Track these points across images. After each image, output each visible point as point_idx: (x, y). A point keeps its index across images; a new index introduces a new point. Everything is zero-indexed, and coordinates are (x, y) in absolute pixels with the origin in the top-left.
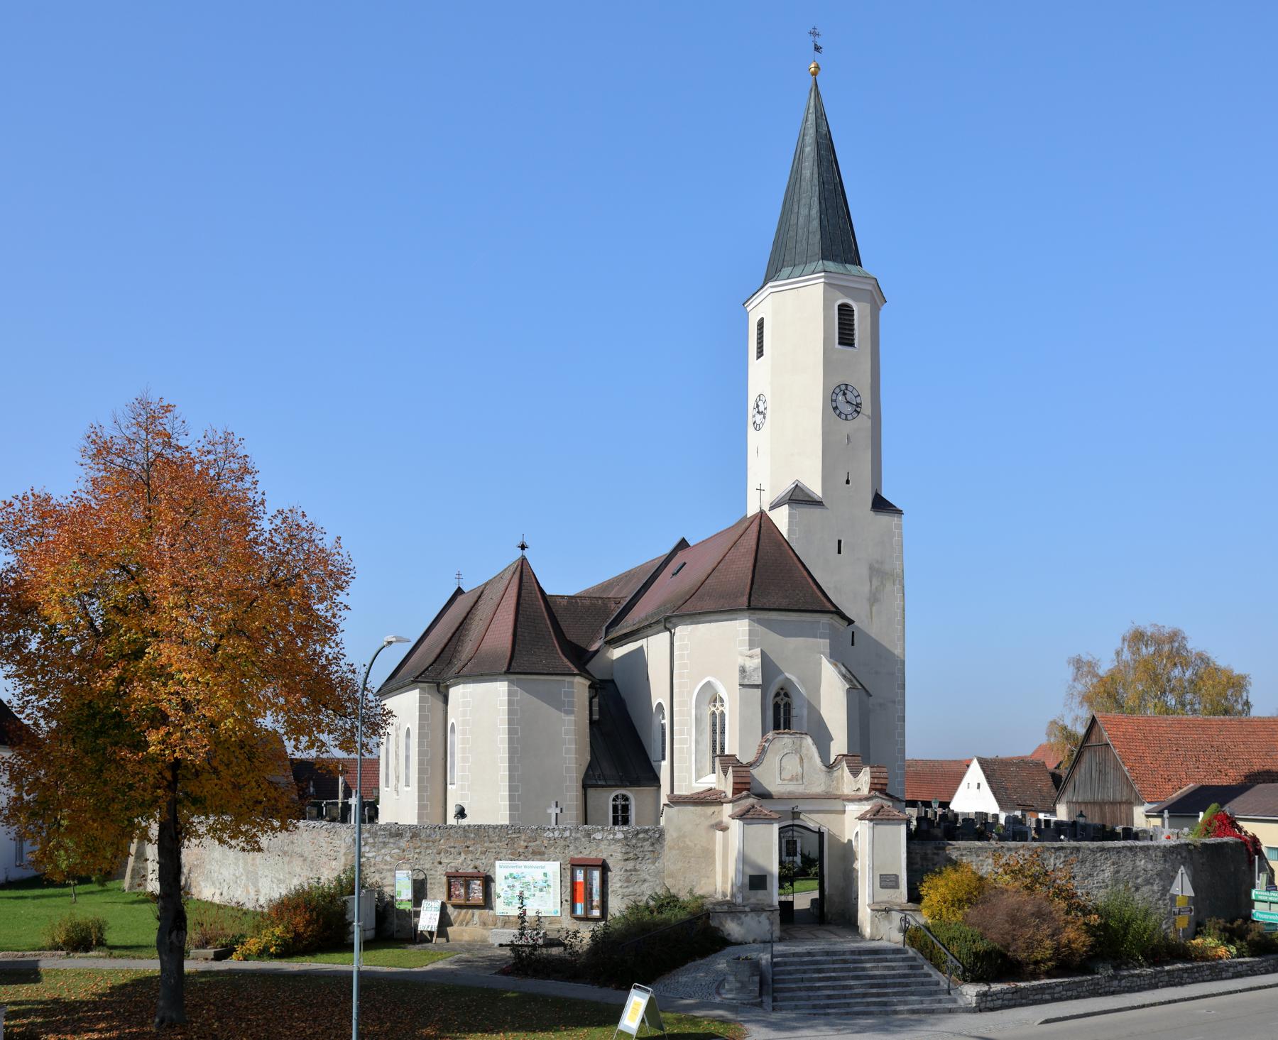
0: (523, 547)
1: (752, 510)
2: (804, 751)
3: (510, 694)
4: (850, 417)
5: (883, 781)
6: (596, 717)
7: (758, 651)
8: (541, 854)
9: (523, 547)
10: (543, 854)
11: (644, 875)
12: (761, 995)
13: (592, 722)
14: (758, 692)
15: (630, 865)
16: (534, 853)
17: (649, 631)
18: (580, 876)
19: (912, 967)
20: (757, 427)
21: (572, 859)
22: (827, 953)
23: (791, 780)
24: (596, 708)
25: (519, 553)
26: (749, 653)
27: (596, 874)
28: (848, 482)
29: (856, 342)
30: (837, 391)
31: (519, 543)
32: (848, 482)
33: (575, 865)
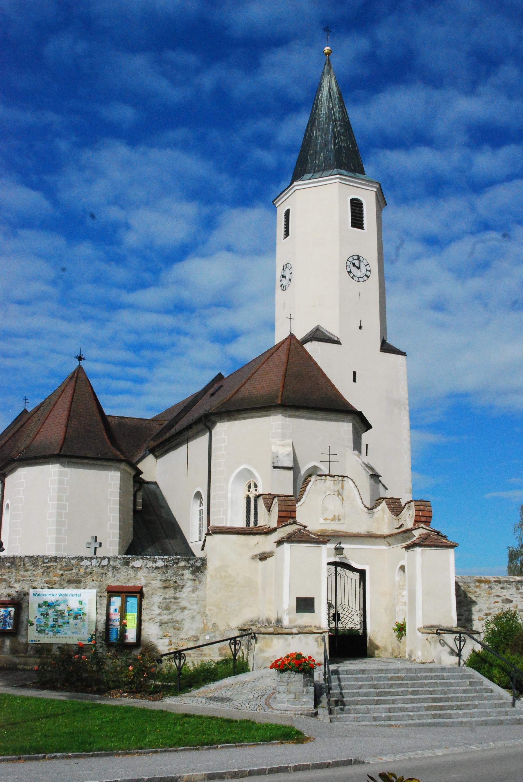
0: (80, 358)
1: (280, 336)
2: (345, 494)
3: (60, 474)
4: (361, 280)
5: (427, 514)
6: (139, 507)
7: (289, 441)
8: (79, 582)
9: (80, 358)
10: (79, 582)
11: (183, 604)
12: (316, 706)
13: (135, 511)
14: (290, 473)
15: (170, 593)
16: (70, 582)
17: (190, 433)
18: (116, 602)
19: (471, 684)
20: (283, 287)
21: (109, 587)
22: (380, 671)
23: (333, 520)
24: (139, 500)
25: (76, 363)
26: (281, 443)
27: (133, 602)
28: (360, 328)
29: (365, 226)
30: (348, 264)
31: (77, 354)
32: (360, 328)
33: (112, 592)
